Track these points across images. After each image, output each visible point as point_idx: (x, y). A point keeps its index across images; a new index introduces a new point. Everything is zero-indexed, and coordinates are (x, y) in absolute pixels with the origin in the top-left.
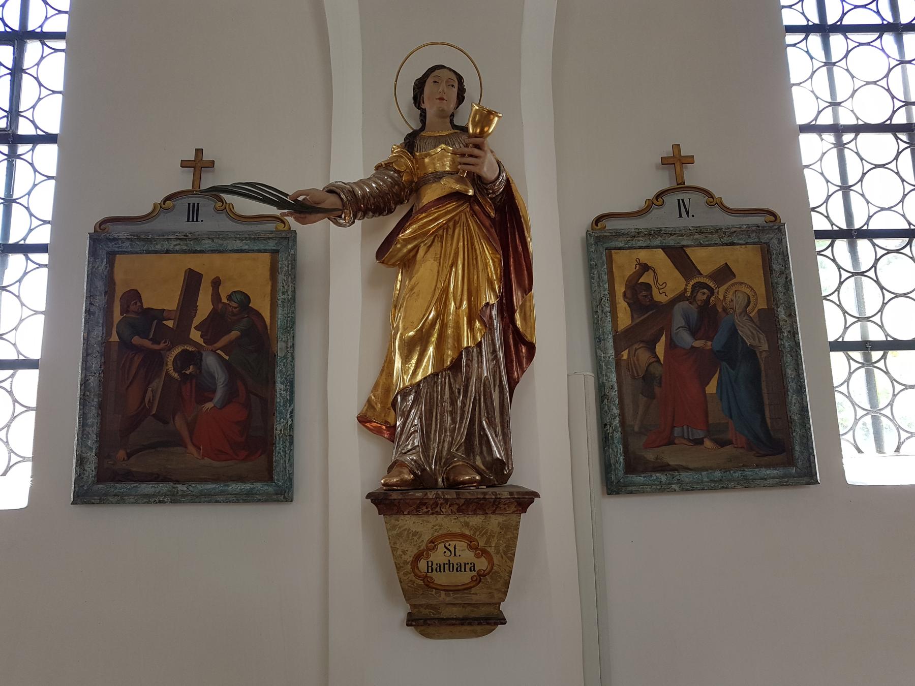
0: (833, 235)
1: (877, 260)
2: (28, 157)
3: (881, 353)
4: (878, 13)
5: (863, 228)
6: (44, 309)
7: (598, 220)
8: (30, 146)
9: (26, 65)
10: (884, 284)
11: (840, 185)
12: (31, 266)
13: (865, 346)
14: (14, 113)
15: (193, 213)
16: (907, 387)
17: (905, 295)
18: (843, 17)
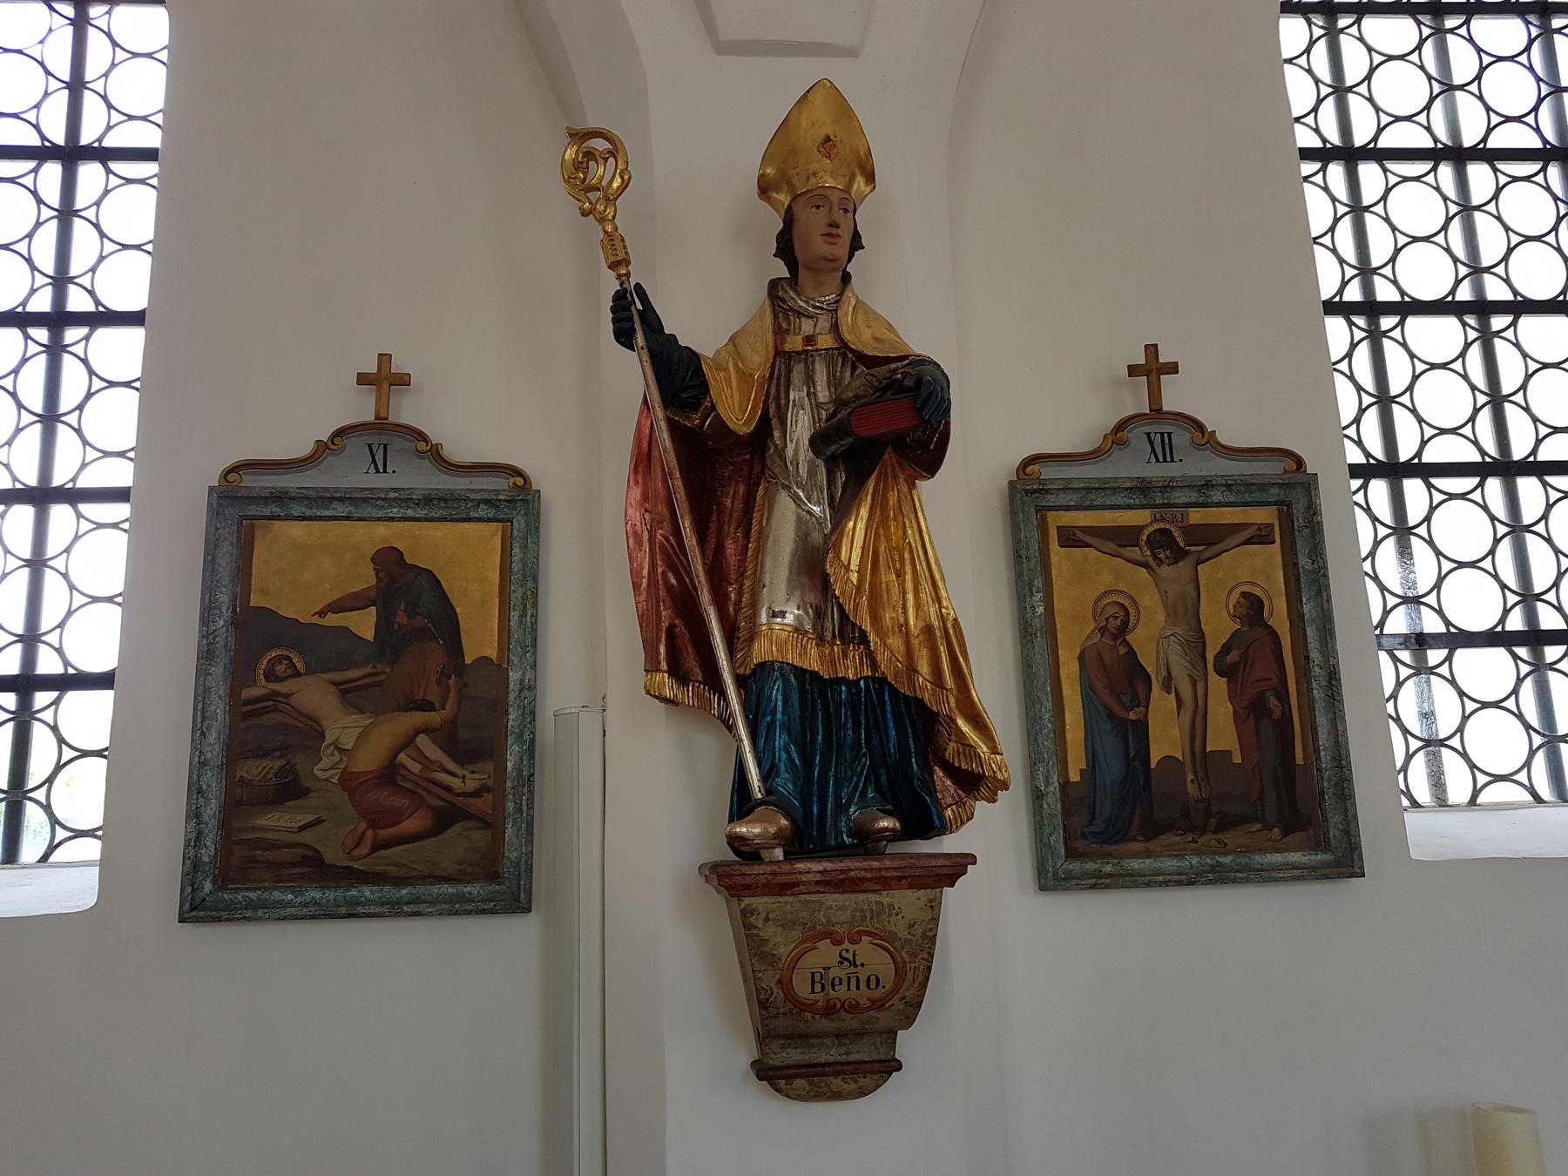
2: (102, 23)
4: (1428, 129)
5: (1335, 300)
6: (118, 587)
8: (84, 331)
9: (88, 76)
12: (114, 181)
13: (1420, 642)
14: (30, 639)
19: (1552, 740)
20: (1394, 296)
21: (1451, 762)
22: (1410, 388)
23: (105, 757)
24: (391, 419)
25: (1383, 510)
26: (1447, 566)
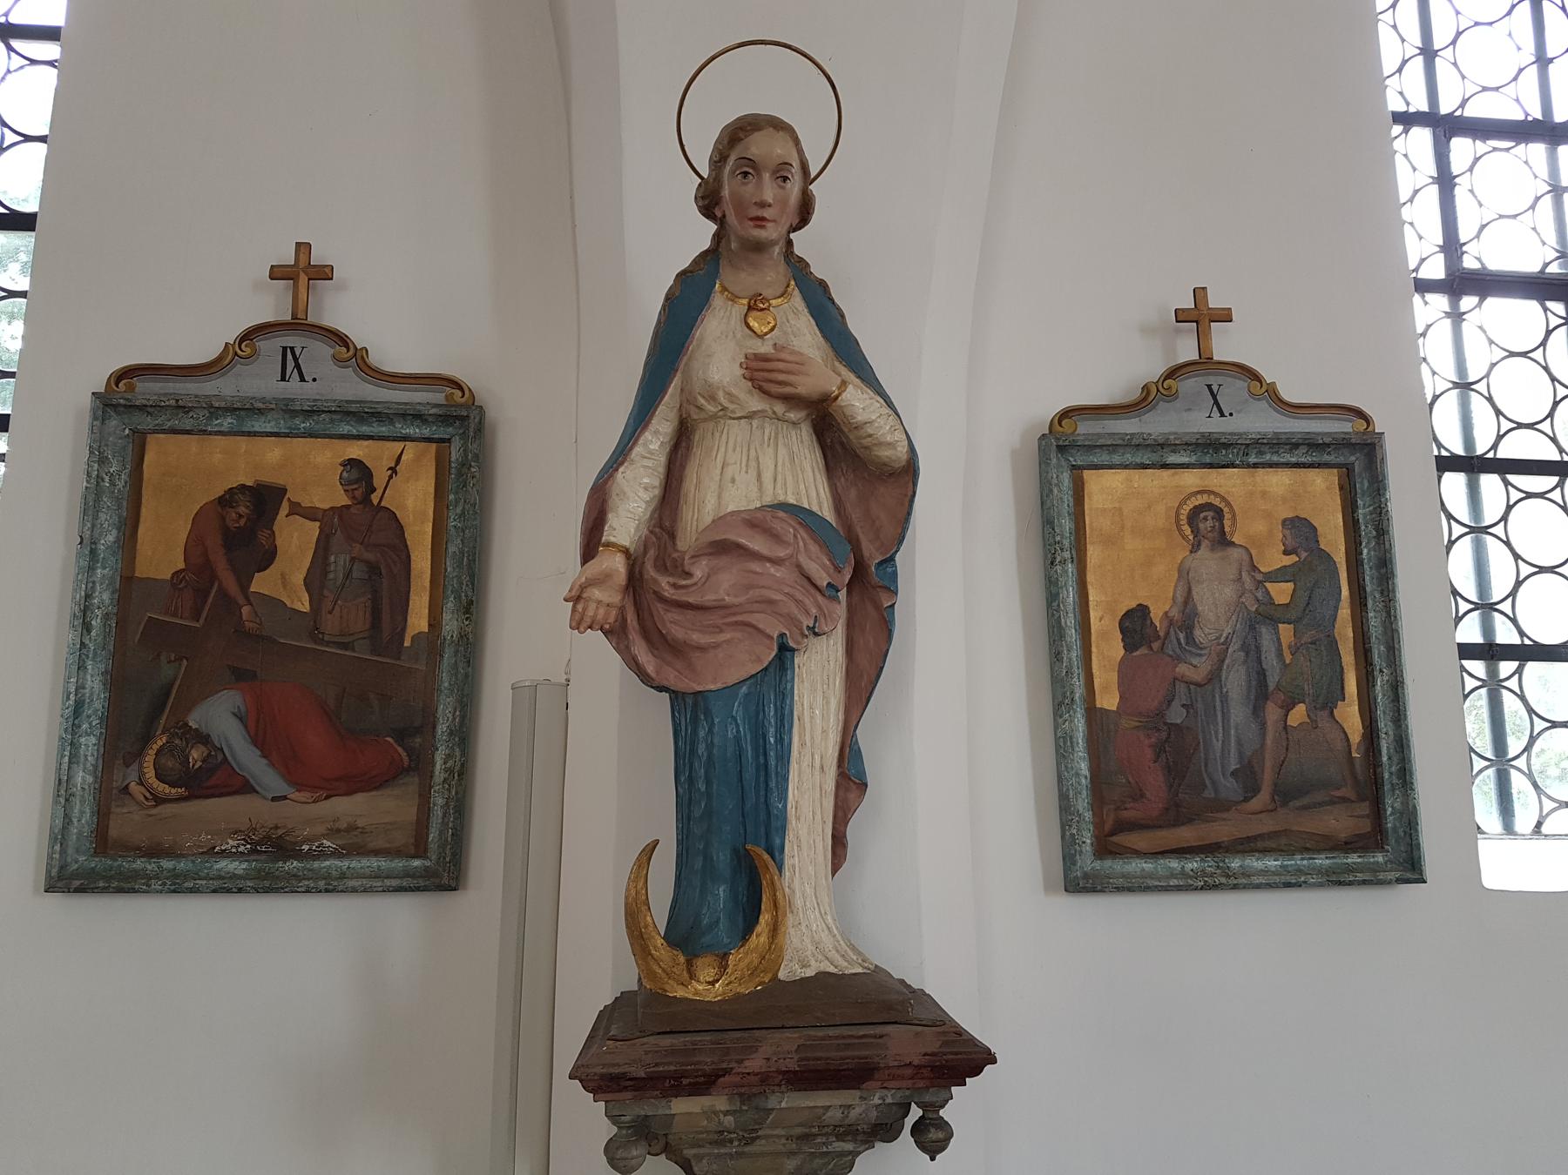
0: (1406, 120)
1: (1519, 584)
3: (1514, 665)
7: (1066, 414)
10: (1511, 517)
11: (1421, 46)
15: (290, 363)
16: (1554, 725)
17: (1551, 570)
18: (1514, 588)
19: (1557, 191)
20: (1515, 639)
21: (1496, 551)
22: (1504, 518)
23: (55, 67)
24: (311, 320)
25: (1459, 509)
26: (1506, 425)
